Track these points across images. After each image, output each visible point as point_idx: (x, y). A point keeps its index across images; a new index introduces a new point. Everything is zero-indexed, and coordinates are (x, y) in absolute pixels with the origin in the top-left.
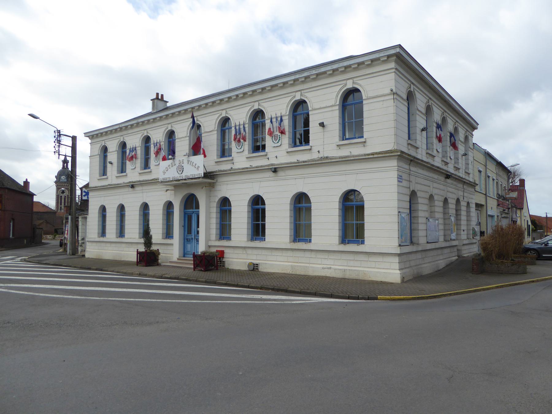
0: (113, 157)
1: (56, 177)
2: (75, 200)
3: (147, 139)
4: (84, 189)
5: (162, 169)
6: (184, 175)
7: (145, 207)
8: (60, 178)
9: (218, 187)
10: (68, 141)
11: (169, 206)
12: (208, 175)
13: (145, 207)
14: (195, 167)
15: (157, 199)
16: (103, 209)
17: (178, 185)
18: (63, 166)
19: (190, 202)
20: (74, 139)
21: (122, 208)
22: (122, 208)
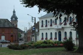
0: (44, 23)
1: (17, 21)
2: (79, 41)
3: (51, 20)
4: (33, 27)
5: (54, 26)
6: (58, 28)
7: (51, 33)
8: (12, 19)
9: (64, 30)
10: (34, 19)
11: (56, 33)
12: (62, 28)
13: (51, 33)
14: (60, 27)
15: (54, 32)
16: (43, 34)
17: (57, 29)
18: (13, 14)
19: (60, 33)
20: (35, 18)
21: (47, 33)
22: (47, 33)
